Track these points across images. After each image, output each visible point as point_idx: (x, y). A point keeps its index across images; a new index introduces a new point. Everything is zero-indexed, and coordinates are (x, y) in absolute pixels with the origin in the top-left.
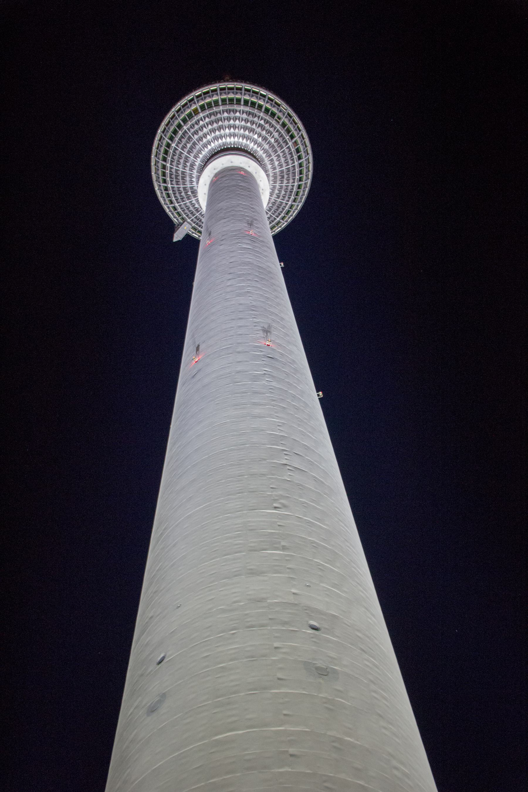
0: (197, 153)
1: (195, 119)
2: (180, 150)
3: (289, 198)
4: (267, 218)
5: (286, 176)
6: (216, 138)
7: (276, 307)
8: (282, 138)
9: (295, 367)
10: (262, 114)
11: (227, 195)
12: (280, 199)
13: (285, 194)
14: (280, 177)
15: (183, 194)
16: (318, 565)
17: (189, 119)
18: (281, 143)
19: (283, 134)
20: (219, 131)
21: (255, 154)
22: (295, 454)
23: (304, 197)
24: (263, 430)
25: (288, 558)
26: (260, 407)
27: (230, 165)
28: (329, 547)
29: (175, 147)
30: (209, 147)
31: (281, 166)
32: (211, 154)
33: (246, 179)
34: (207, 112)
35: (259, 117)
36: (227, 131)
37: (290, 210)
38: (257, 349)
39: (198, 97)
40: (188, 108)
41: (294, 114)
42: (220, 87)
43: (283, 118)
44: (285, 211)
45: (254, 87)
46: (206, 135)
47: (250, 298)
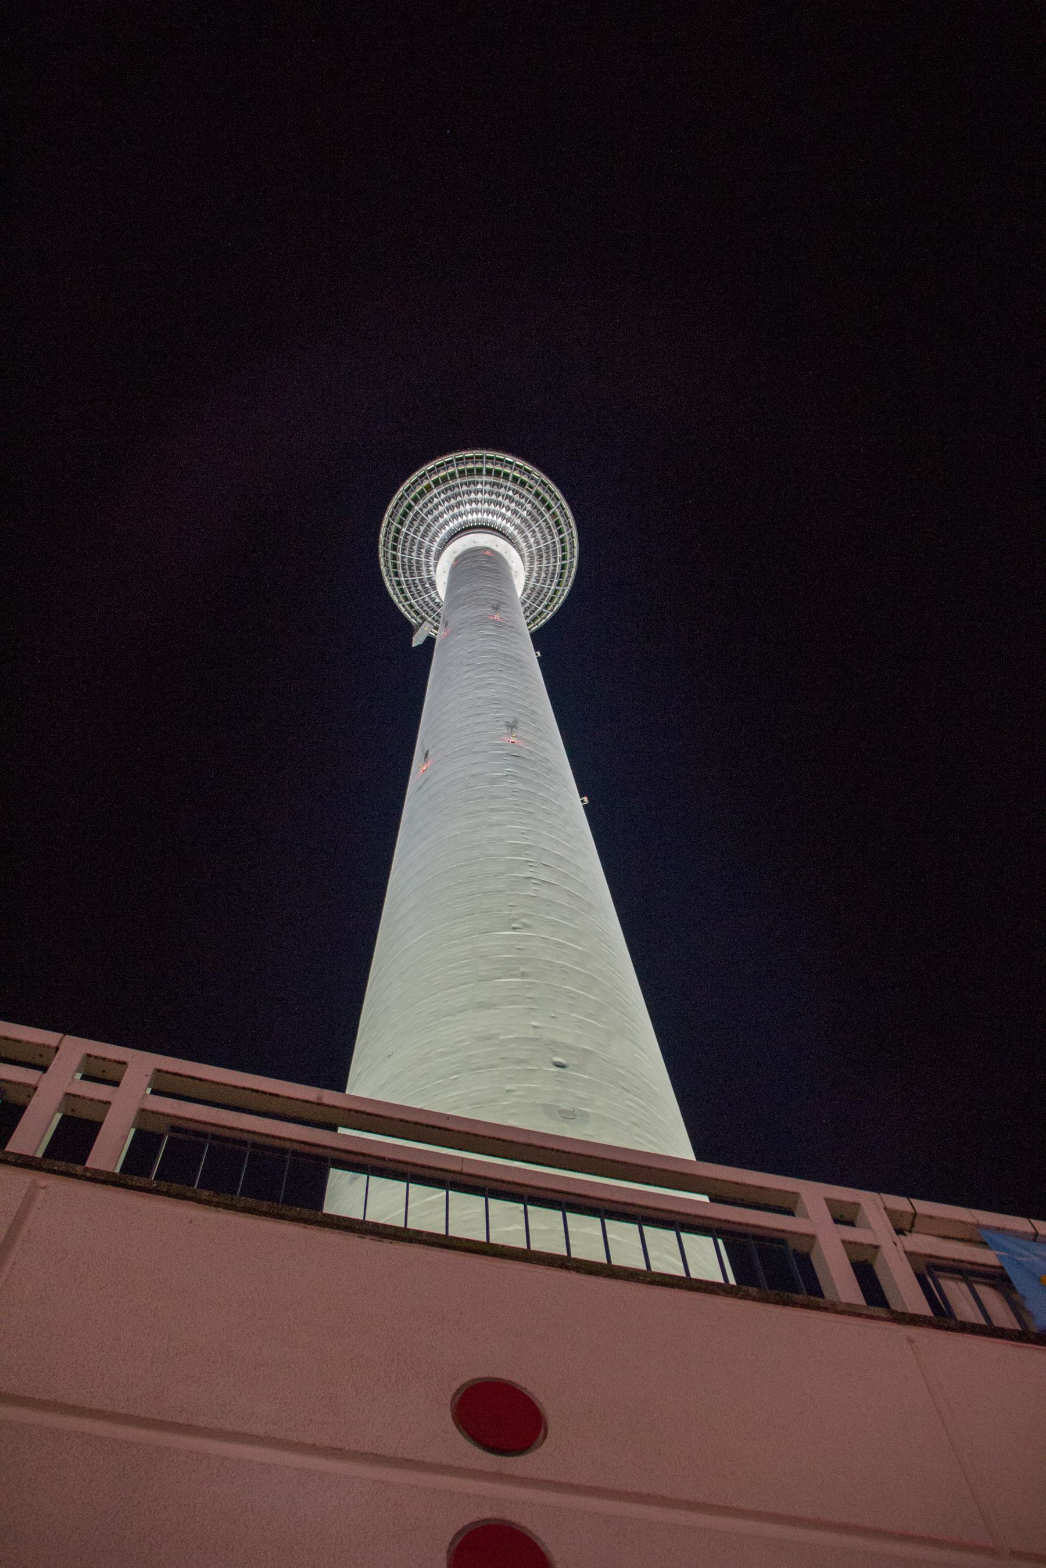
1: (427, 496)
2: (412, 534)
3: (552, 581)
5: (545, 555)
8: (536, 510)
10: (509, 484)
11: (468, 579)
13: (546, 577)
14: (538, 557)
15: (420, 587)
18: (535, 516)
22: (543, 866)
23: (571, 580)
24: (502, 840)
25: (527, 986)
26: (500, 813)
27: (472, 545)
29: (406, 533)
35: (506, 488)
36: (468, 507)
39: (429, 471)
42: (456, 457)
46: (442, 514)
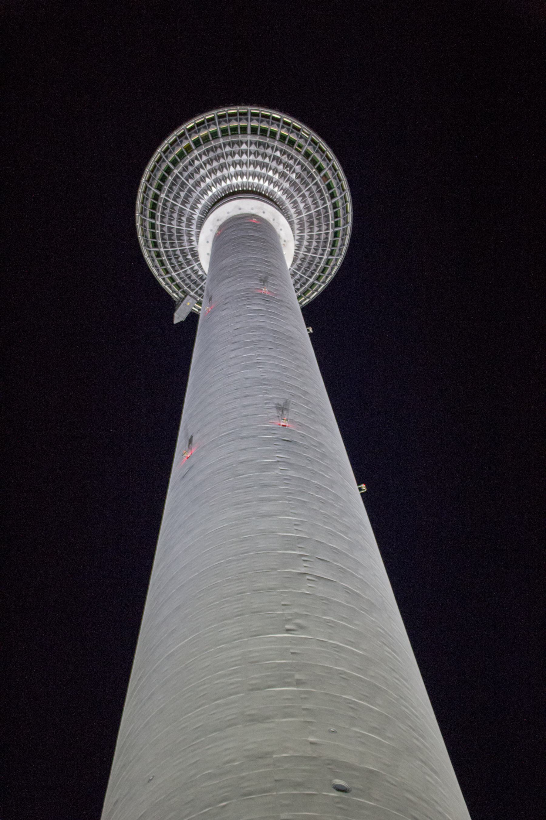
0: (195, 203)
1: (187, 158)
2: (171, 201)
4: (290, 275)
6: (218, 181)
7: (297, 379)
8: (306, 172)
9: (323, 451)
10: (276, 144)
12: (311, 252)
13: (317, 246)
14: (308, 224)
16: (349, 703)
17: (181, 160)
19: (308, 166)
20: (221, 171)
21: (271, 197)
23: (345, 248)
25: (303, 696)
27: (237, 212)
28: (365, 678)
29: (165, 199)
30: (210, 194)
31: (308, 208)
32: (213, 202)
33: (259, 228)
34: (204, 148)
35: (272, 148)
36: (232, 170)
37: (326, 266)
38: (269, 431)
39: (189, 130)
40: (178, 145)
41: (320, 140)
42: (219, 114)
43: (305, 146)
44: (320, 269)
45: (264, 110)
46: (204, 178)
47: (261, 370)
